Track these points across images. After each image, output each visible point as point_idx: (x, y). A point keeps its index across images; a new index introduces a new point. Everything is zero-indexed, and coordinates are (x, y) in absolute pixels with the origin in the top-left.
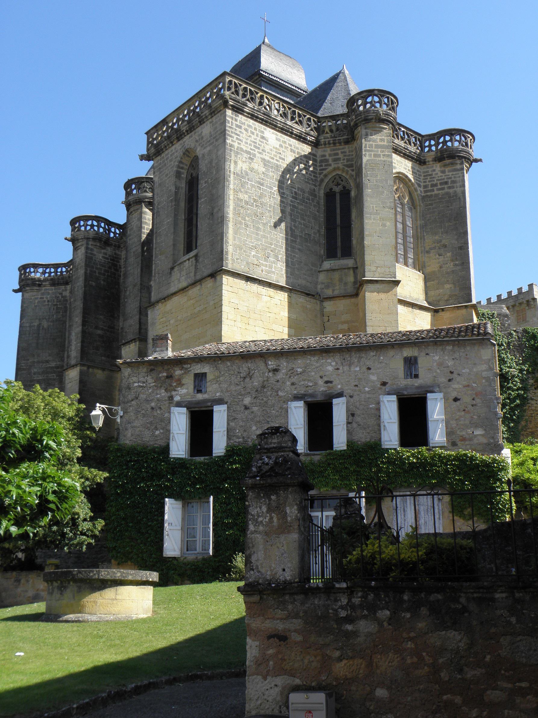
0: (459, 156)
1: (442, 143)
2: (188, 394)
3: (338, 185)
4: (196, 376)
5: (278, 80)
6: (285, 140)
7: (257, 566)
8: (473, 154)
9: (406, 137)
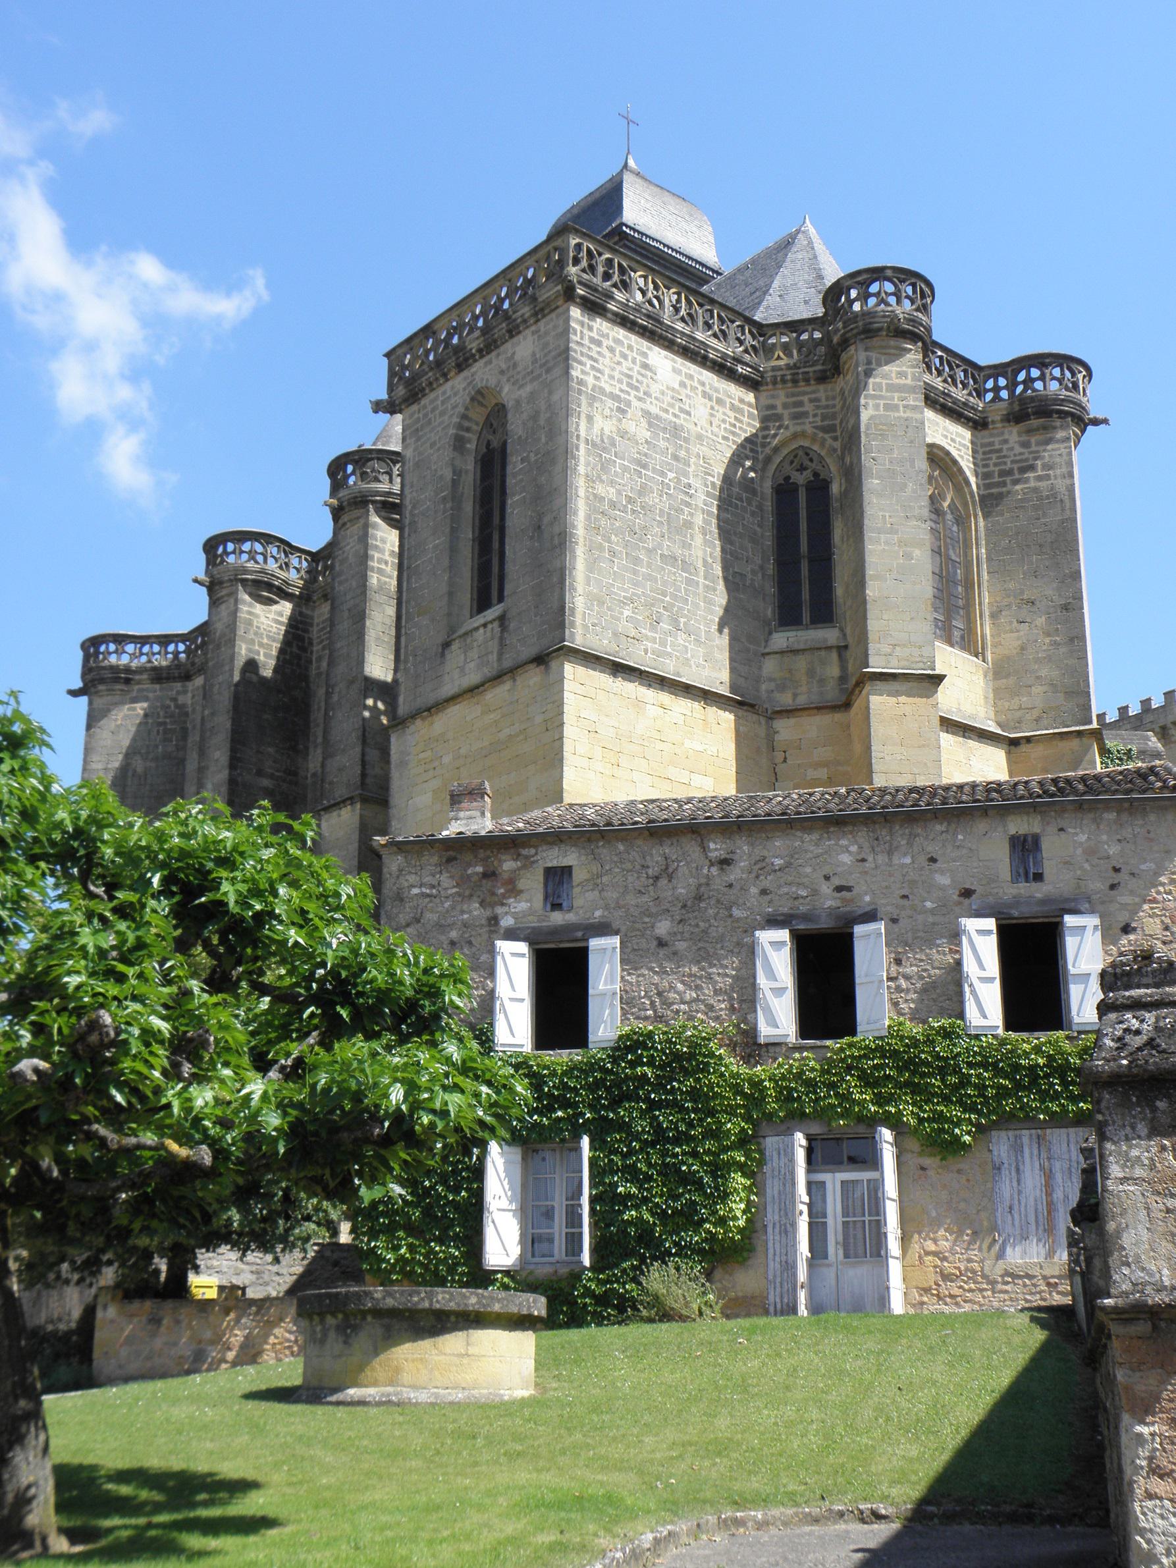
0: (1059, 412)
1: (1024, 382)
2: (531, 912)
3: (802, 469)
4: (550, 872)
5: (661, 247)
6: (692, 372)
7: (1137, 1256)
8: (1089, 407)
9: (947, 369)
